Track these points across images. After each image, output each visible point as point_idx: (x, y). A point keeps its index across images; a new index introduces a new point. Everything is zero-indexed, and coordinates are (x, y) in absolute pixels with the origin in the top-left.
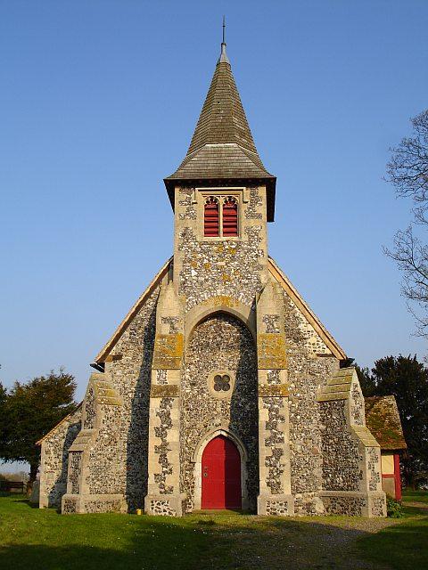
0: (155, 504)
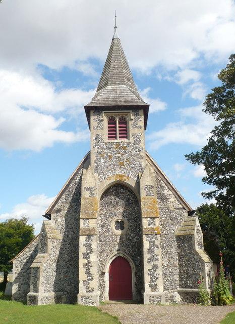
0: (84, 299)
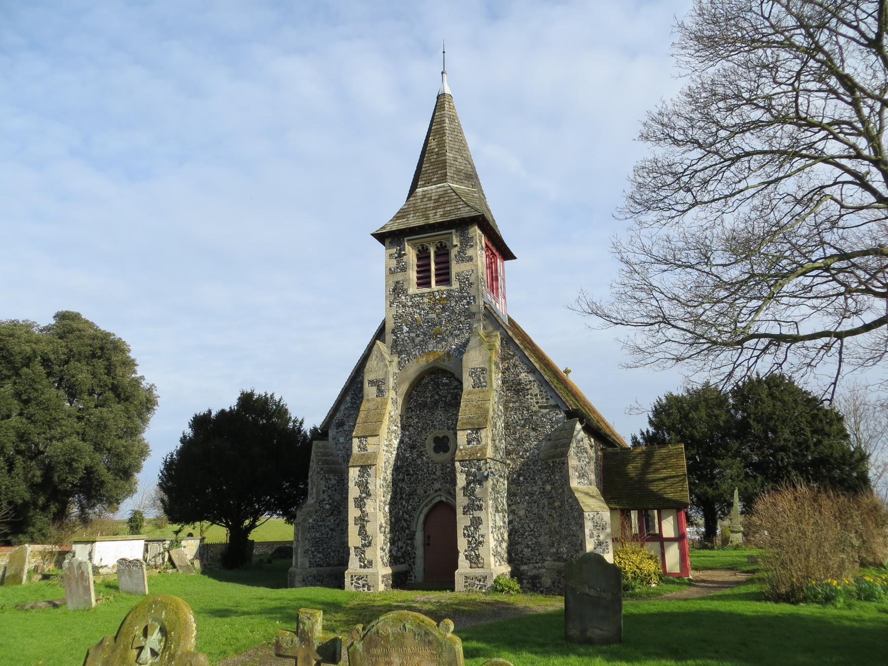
0: (355, 579)
